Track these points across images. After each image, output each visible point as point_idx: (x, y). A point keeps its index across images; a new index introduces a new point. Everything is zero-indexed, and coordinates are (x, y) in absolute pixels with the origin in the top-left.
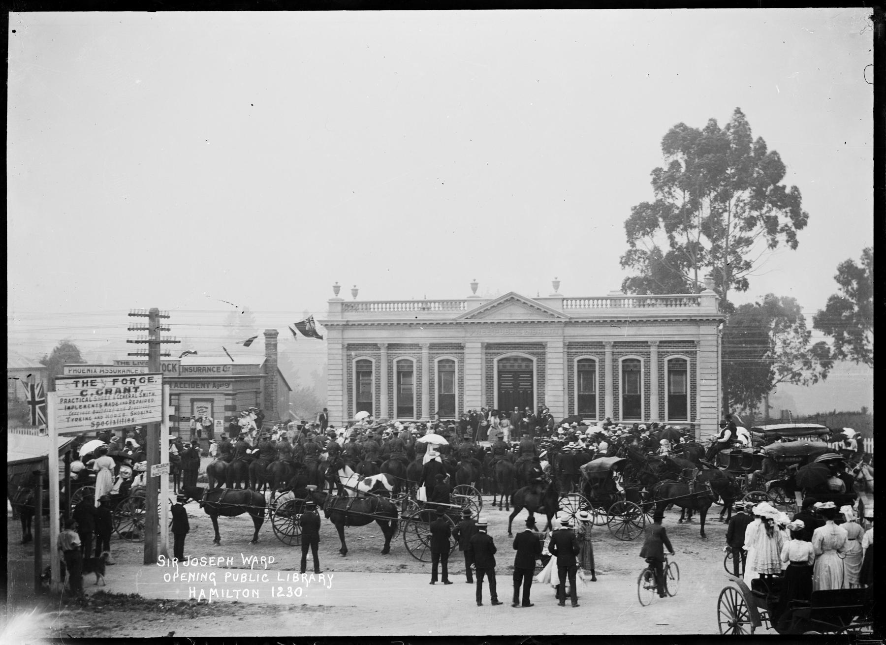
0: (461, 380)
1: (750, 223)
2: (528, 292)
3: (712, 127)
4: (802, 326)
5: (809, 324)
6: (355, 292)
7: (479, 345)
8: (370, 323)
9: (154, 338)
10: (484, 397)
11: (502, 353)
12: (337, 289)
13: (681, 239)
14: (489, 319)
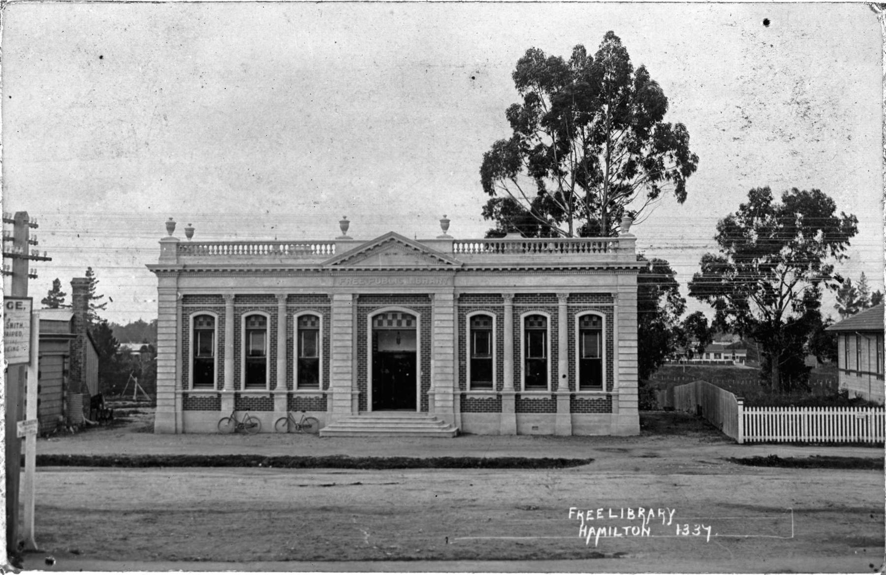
0: (327, 341)
1: (630, 170)
2: (412, 231)
3: (580, 52)
4: (675, 292)
5: (684, 291)
6: (190, 233)
7: (350, 297)
8: (213, 269)
9: (21, 251)
10: (355, 362)
11: (378, 308)
12: (171, 227)
13: (551, 185)
14: (363, 265)
